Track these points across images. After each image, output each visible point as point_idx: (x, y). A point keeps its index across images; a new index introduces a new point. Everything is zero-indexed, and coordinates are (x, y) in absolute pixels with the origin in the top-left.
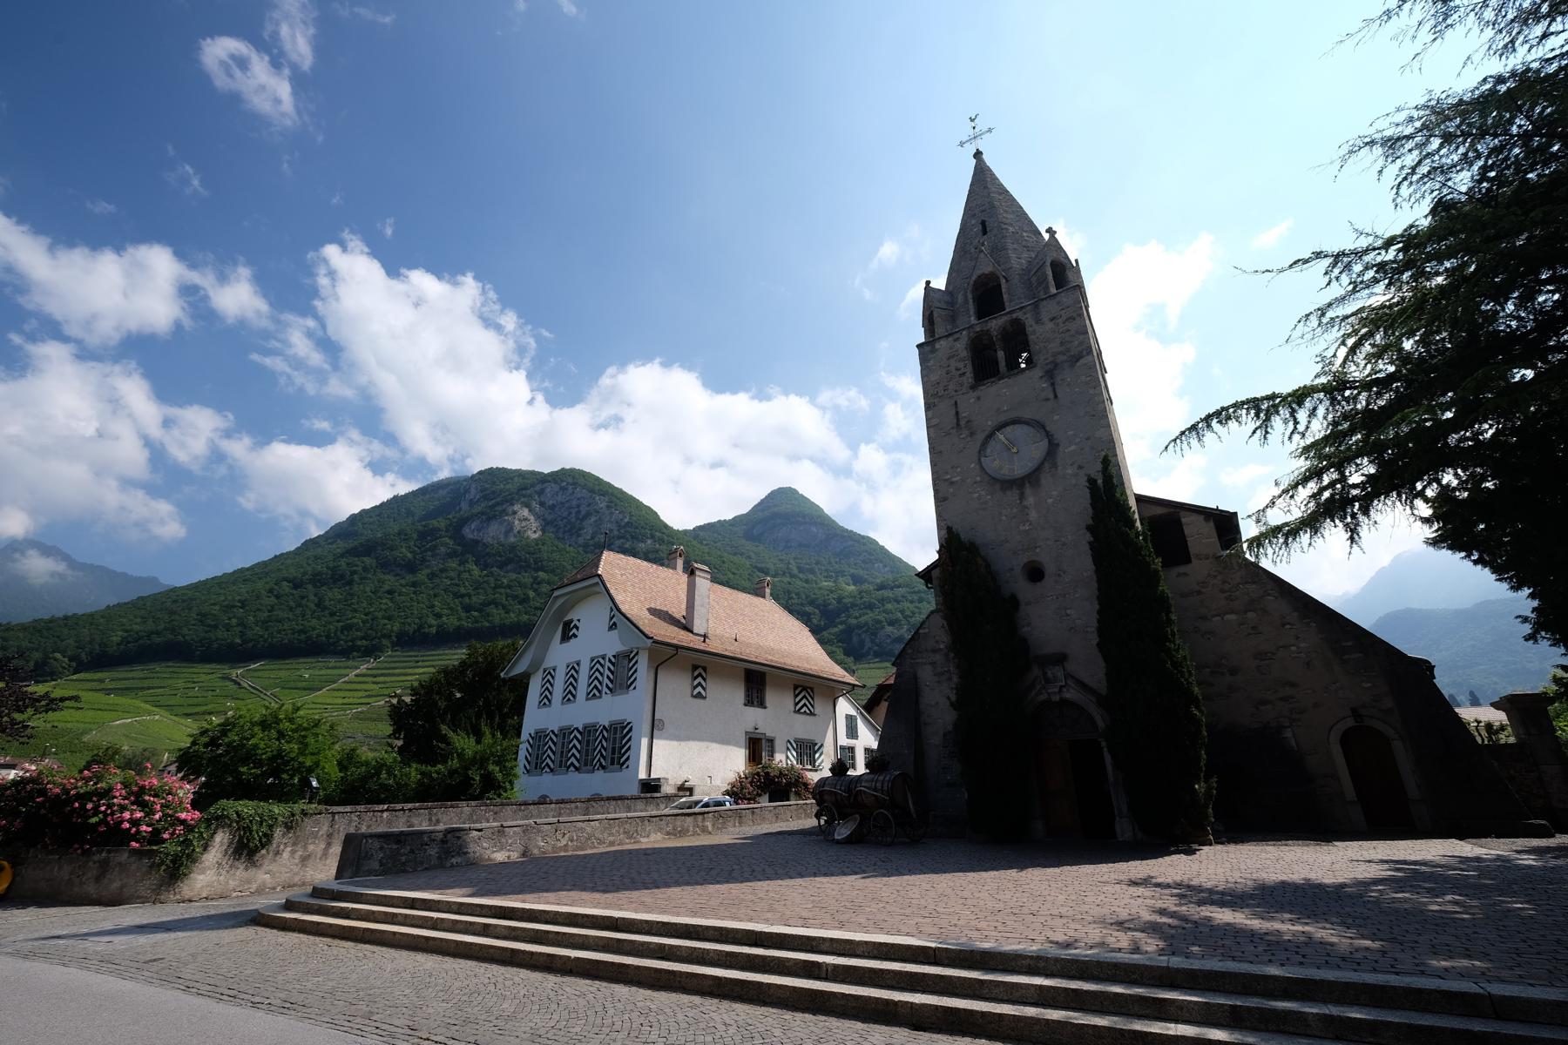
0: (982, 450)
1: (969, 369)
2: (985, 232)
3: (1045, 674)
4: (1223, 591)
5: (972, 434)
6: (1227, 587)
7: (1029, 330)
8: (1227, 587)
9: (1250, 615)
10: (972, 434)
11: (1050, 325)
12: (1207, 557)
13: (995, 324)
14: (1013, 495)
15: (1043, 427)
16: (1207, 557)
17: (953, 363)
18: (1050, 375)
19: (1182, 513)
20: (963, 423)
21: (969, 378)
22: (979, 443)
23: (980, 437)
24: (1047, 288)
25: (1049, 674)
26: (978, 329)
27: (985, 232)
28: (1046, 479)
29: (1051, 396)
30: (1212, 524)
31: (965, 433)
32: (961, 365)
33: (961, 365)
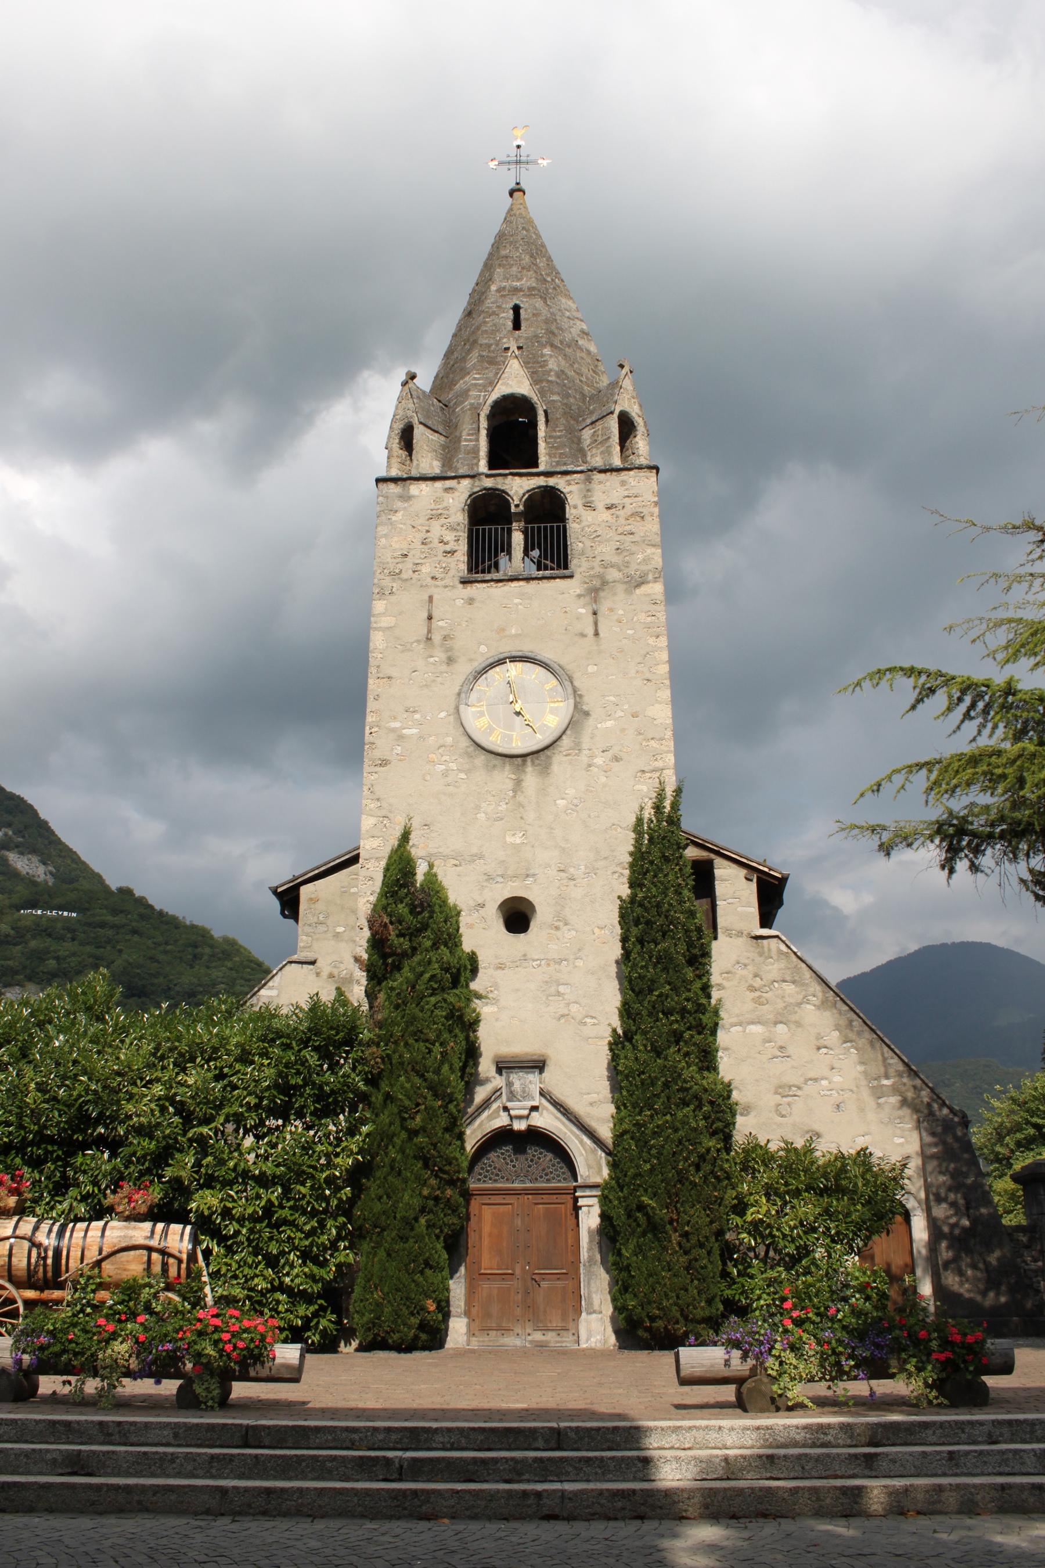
0: (462, 694)
1: (463, 547)
2: (517, 325)
3: (510, 1084)
4: (752, 989)
5: (450, 661)
6: (758, 982)
7: (570, 513)
8: (758, 982)
9: (781, 1027)
10: (450, 661)
11: (606, 516)
12: (740, 934)
13: (517, 487)
14: (504, 777)
15: (571, 680)
16: (740, 934)
17: (437, 529)
18: (595, 592)
19: (718, 861)
20: (437, 638)
21: (460, 562)
22: (460, 679)
23: (464, 669)
24: (608, 452)
25: (517, 1086)
26: (489, 483)
27: (517, 325)
28: (559, 762)
29: (590, 631)
30: (754, 886)
31: (440, 656)
32: (449, 537)
33: (449, 537)
